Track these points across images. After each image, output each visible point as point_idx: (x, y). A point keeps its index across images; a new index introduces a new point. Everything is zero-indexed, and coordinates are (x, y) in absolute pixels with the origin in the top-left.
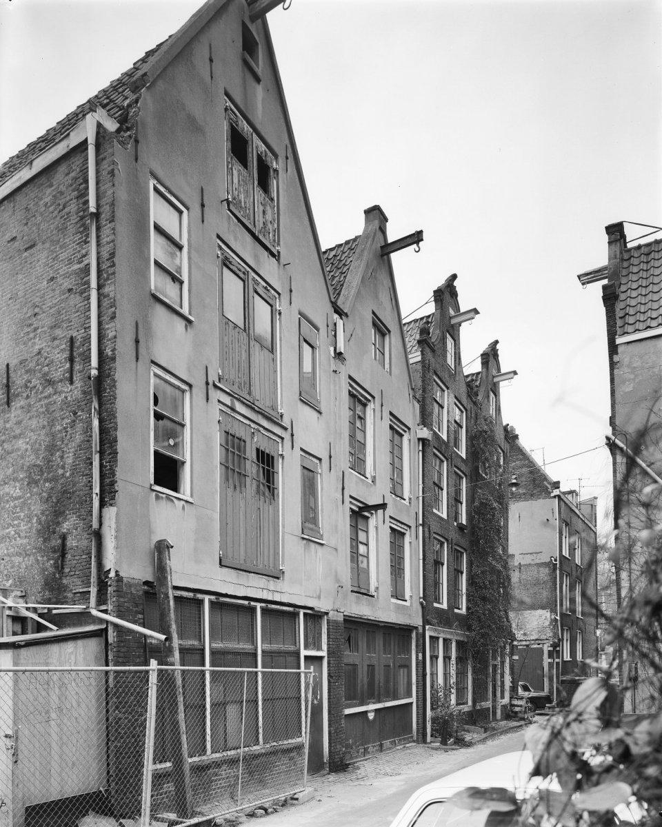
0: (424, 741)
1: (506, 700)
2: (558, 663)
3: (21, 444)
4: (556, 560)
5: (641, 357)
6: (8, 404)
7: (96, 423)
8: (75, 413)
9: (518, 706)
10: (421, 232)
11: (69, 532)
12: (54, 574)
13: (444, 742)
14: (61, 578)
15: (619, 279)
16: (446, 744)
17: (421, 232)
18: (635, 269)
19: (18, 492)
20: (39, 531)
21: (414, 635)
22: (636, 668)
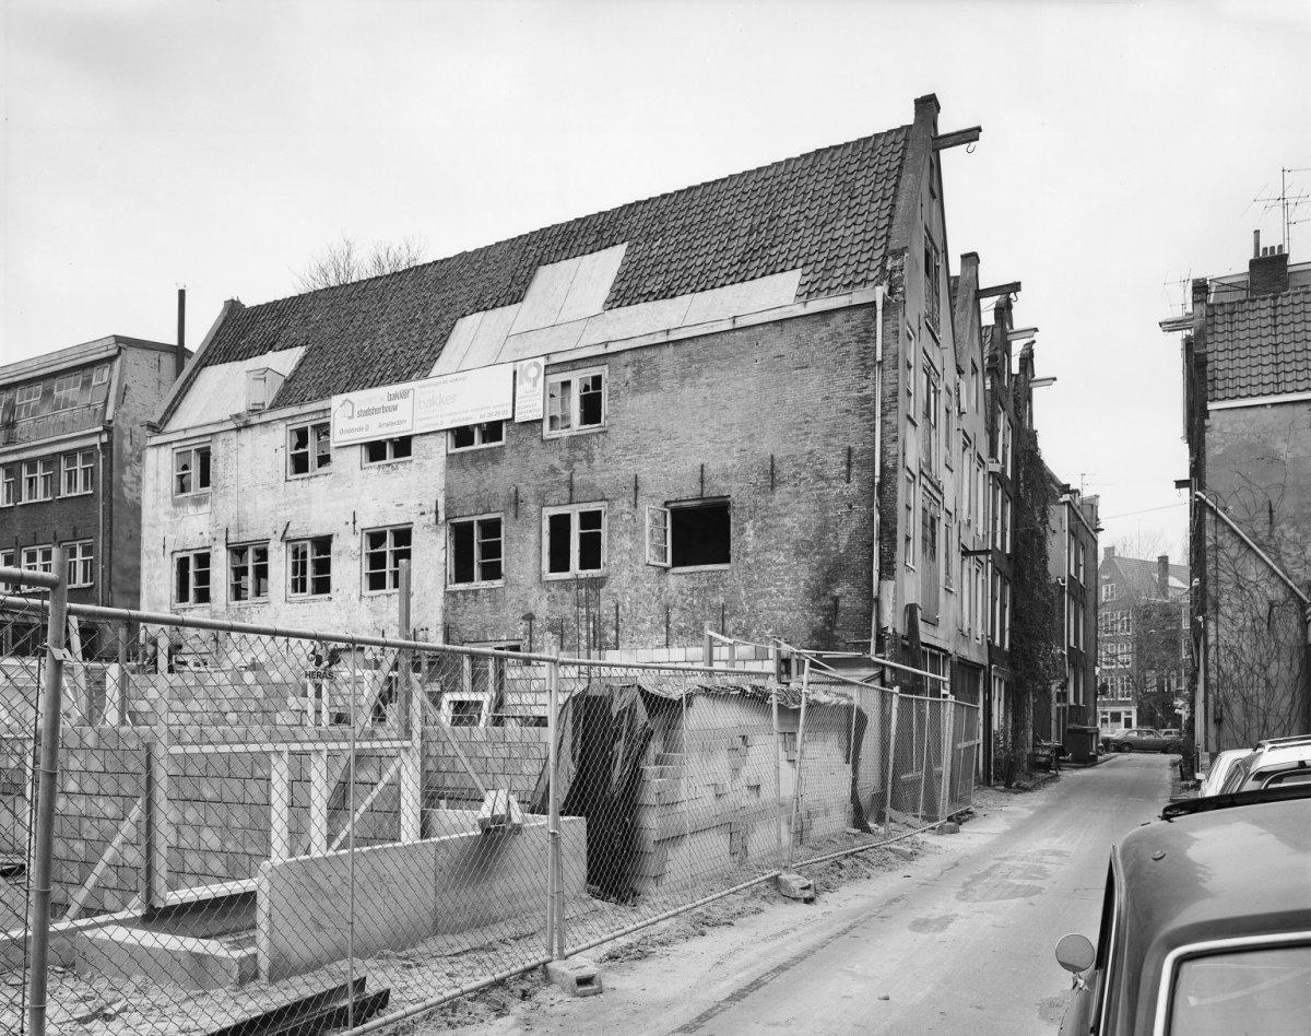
0: (989, 785)
1: (1029, 750)
2: (1064, 708)
3: (787, 521)
4: (1063, 581)
5: (1231, 424)
6: (772, 488)
7: (877, 517)
8: (850, 507)
9: (1042, 756)
10: (1019, 283)
11: (841, 596)
12: (824, 627)
13: (1008, 785)
14: (831, 631)
15: (1204, 338)
16: (1010, 787)
17: (1019, 283)
18: (1220, 329)
19: (782, 559)
20: (806, 593)
21: (982, 674)
22: (1221, 710)
